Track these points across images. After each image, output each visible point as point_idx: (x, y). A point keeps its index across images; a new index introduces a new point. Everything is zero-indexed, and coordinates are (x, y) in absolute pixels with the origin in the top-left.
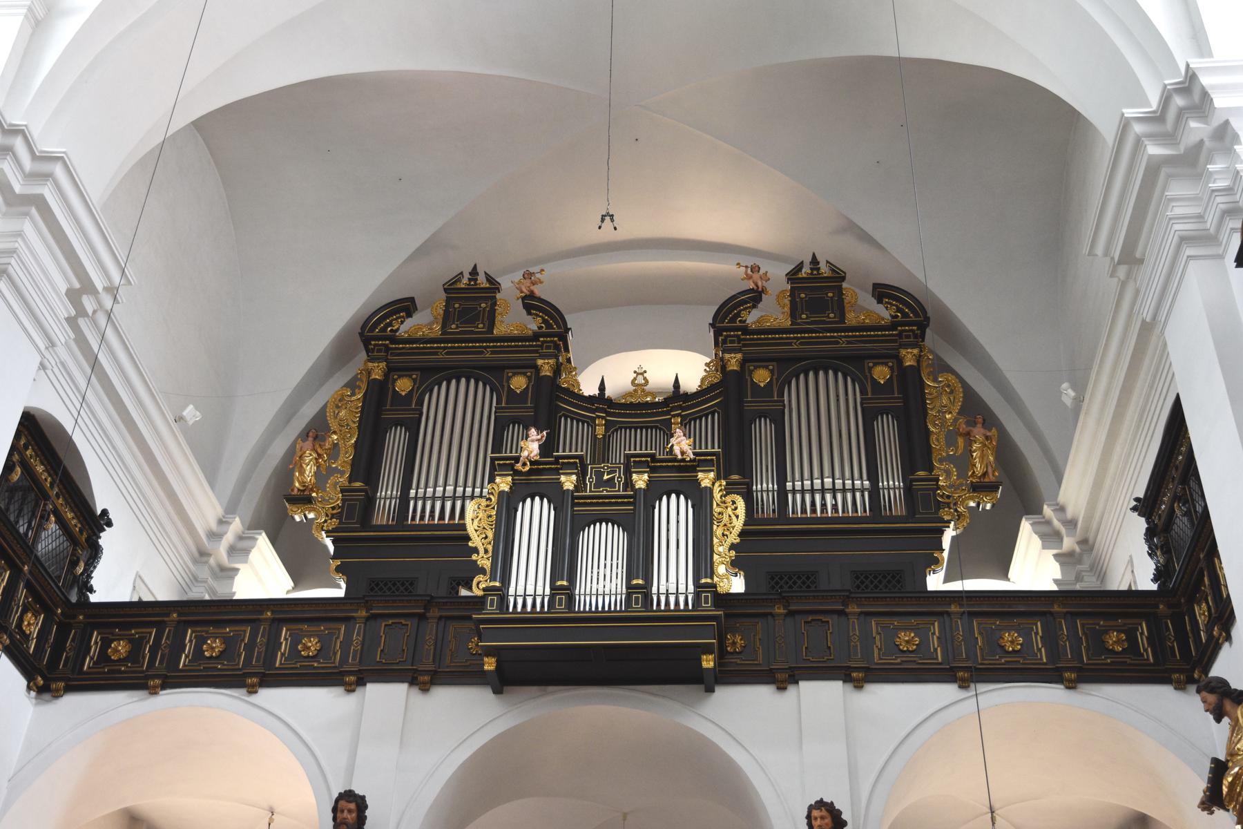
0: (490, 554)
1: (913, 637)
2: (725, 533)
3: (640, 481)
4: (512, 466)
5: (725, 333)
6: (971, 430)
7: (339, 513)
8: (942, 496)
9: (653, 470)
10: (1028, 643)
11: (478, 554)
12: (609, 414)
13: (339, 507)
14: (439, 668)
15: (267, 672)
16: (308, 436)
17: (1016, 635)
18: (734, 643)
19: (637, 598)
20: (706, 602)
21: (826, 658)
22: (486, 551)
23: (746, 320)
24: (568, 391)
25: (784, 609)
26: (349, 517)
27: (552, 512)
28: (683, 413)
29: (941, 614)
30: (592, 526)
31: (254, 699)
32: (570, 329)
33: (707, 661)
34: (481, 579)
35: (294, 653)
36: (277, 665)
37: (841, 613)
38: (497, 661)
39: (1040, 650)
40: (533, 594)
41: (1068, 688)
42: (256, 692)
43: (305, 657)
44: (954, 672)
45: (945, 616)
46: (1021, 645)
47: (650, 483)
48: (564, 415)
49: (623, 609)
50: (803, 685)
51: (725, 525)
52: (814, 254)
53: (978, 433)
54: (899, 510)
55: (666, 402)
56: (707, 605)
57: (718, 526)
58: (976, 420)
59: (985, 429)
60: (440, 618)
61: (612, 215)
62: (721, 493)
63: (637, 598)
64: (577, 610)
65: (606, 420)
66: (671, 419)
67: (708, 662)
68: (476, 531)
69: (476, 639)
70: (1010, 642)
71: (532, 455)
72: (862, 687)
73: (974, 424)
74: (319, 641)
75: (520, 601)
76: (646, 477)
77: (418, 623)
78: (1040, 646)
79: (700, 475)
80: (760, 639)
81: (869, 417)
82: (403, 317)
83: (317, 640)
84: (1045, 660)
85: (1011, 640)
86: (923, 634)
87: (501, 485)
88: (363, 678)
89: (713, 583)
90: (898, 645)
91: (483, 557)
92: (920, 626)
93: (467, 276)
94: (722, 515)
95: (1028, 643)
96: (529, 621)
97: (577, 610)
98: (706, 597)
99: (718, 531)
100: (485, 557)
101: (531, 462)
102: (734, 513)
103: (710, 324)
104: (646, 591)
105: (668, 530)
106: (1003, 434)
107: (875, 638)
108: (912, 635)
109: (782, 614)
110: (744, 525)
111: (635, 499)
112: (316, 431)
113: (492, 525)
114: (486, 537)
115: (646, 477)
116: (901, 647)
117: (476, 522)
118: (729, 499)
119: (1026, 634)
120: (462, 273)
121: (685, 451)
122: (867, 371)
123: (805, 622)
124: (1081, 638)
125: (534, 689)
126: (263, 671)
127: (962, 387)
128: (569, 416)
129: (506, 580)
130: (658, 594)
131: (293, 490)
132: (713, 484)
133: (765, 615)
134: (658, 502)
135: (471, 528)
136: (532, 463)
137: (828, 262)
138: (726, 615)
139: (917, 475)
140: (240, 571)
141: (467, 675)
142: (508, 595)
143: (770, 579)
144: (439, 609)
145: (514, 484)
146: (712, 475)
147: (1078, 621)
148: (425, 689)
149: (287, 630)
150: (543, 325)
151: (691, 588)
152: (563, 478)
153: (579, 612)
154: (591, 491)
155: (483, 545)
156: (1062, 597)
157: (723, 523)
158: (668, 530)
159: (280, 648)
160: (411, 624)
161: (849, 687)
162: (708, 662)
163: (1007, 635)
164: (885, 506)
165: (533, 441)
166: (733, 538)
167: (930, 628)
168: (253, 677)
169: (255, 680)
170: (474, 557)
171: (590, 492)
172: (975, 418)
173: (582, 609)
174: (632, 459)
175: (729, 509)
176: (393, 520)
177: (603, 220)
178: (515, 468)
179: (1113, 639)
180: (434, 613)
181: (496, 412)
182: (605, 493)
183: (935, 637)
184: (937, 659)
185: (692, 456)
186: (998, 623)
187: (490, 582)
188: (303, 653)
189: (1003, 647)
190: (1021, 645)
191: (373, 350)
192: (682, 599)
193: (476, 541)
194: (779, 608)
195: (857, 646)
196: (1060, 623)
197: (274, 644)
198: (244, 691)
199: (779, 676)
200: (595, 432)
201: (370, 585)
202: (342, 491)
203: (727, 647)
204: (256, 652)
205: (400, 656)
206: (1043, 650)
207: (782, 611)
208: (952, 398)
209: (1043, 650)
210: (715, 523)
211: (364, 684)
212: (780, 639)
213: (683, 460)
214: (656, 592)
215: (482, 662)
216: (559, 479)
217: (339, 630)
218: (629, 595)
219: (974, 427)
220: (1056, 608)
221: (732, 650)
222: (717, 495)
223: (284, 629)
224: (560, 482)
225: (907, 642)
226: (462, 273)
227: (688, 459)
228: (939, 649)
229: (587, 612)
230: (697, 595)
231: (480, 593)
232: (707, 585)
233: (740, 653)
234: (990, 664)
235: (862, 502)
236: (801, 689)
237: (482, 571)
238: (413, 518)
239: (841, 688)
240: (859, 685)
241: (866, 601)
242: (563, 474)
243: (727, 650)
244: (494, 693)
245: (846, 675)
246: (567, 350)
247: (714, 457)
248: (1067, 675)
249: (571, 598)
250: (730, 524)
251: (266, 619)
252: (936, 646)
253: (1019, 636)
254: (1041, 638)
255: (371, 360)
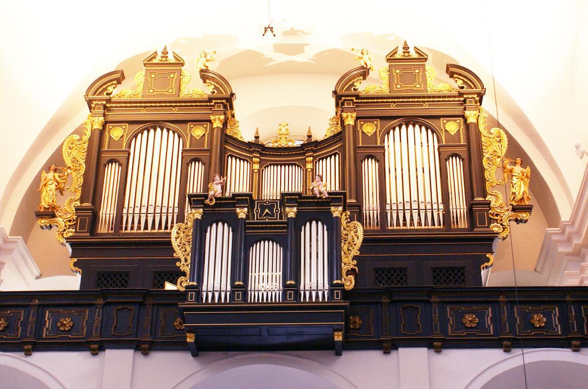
0: (189, 261)
1: (474, 318)
2: (350, 248)
3: (292, 212)
4: (202, 202)
5: (344, 98)
6: (513, 169)
7: (74, 224)
8: (492, 215)
9: (300, 204)
10: (549, 322)
11: (181, 262)
12: (262, 155)
13: (74, 221)
14: (154, 339)
15: (38, 341)
16: (50, 169)
17: (542, 316)
18: (355, 322)
19: (290, 294)
20: (337, 296)
21: (416, 332)
22: (186, 260)
23: (358, 89)
24: (230, 137)
25: (388, 299)
26: (82, 227)
27: (231, 234)
28: (314, 155)
29: (493, 302)
30: (259, 243)
31: (29, 359)
32: (234, 94)
33: (337, 336)
34: (183, 280)
35: (55, 328)
36: (44, 336)
37: (427, 302)
38: (195, 336)
39: (557, 326)
40: (219, 290)
41: (574, 351)
42: (30, 355)
43: (62, 331)
44: (500, 341)
45: (496, 303)
46: (545, 323)
47: (297, 214)
48: (230, 155)
49: (281, 301)
50: (401, 350)
51: (349, 243)
52: (405, 42)
53: (518, 169)
54: (463, 224)
55: (303, 146)
56: (338, 299)
57: (344, 243)
58: (516, 161)
59: (522, 167)
60: (154, 305)
61: (272, 28)
62: (346, 221)
63: (290, 294)
64: (249, 302)
65: (260, 159)
66: (305, 159)
67: (338, 337)
68: (179, 246)
69: (179, 319)
70: (538, 321)
71: (216, 194)
72: (440, 351)
73: (515, 164)
74: (72, 320)
75: (210, 295)
76: (295, 209)
77: (139, 308)
78: (557, 323)
79: (333, 209)
80: (372, 320)
81: (444, 157)
82: (115, 84)
83: (70, 320)
84: (560, 333)
85: (538, 319)
86: (481, 315)
87: (196, 215)
88: (102, 346)
89: (342, 284)
90: (464, 323)
91: (184, 265)
92: (479, 311)
93: (160, 54)
94: (347, 235)
95: (549, 322)
96: (216, 310)
97: (249, 302)
98: (337, 293)
99: (345, 247)
100: (185, 264)
101: (215, 198)
102: (355, 235)
103: (333, 91)
104: (296, 288)
105: (311, 246)
106: (534, 171)
107: (449, 319)
108: (474, 316)
109: (386, 303)
110: (362, 243)
111: (288, 225)
112: (56, 163)
113: (189, 242)
114: (186, 251)
115: (295, 209)
116: (467, 325)
117: (178, 240)
118: (351, 225)
119: (548, 315)
120: (156, 52)
121: (322, 192)
122: (442, 125)
123: (403, 308)
124: (584, 318)
125: (220, 353)
126: (35, 340)
127: (508, 137)
128: (234, 156)
129: (200, 280)
130: (305, 291)
131: (40, 208)
132: (341, 215)
133: (377, 303)
134: (303, 227)
135: (175, 244)
136: (217, 199)
137: (415, 47)
138: (351, 304)
139: (475, 201)
140: (6, 265)
141: (175, 344)
142: (202, 291)
143: (376, 272)
144: (153, 299)
145: (204, 214)
146: (341, 208)
147: (582, 307)
148: (146, 353)
149: (49, 313)
150: (215, 91)
151: (229, 288)
152: (238, 210)
153: (251, 303)
154: (257, 219)
155: (184, 256)
156: (572, 291)
157: (347, 242)
158: (311, 246)
159: (45, 325)
160: (135, 309)
161: (432, 351)
162: (338, 337)
163: (536, 316)
164: (454, 221)
165: (217, 184)
166: (355, 252)
167: (485, 312)
168: (28, 345)
169: (30, 347)
170: (178, 264)
171: (257, 220)
172: (516, 160)
173: (253, 301)
174: (286, 197)
175: (352, 232)
176: (112, 230)
177: (266, 31)
178: (205, 202)
179: (538, 319)
180: (150, 301)
181: (182, 153)
182: (267, 220)
183: (489, 318)
184: (490, 332)
185: (327, 196)
186: (530, 308)
187: (190, 281)
188: (61, 328)
189: (533, 325)
190: (545, 323)
191: (94, 108)
192: (320, 294)
193: (179, 253)
194: (385, 299)
195: (437, 324)
196: (571, 308)
197: (40, 323)
198: (22, 354)
199: (385, 345)
200: (252, 167)
201: (98, 276)
202: (76, 209)
203: (350, 325)
204: (29, 327)
205: (128, 331)
206: (559, 326)
207: (387, 300)
208: (500, 145)
209: (559, 326)
210: (343, 241)
211: (104, 350)
212: (386, 320)
213: (321, 198)
214: (303, 289)
215: (184, 335)
216: (235, 210)
217: (85, 312)
218: (284, 292)
219: (515, 166)
220: (568, 298)
221: (353, 327)
222: (344, 222)
223: (47, 312)
224: (236, 213)
225: (471, 321)
226: (156, 52)
227: (324, 197)
228: (491, 326)
229: (256, 303)
230: (331, 292)
231: (183, 289)
232: (338, 285)
233: (359, 329)
234: (524, 336)
235: (439, 214)
236: (400, 355)
237: (184, 274)
238: (126, 229)
239: (427, 354)
240: (438, 350)
241: (443, 294)
242: (238, 207)
243: (350, 327)
244: (193, 356)
245: (430, 344)
246: (232, 108)
247: (342, 196)
248: (574, 342)
249: (245, 293)
250: (353, 242)
251: (35, 305)
252: (489, 324)
253: (544, 317)
254: (558, 318)
255: (93, 115)
